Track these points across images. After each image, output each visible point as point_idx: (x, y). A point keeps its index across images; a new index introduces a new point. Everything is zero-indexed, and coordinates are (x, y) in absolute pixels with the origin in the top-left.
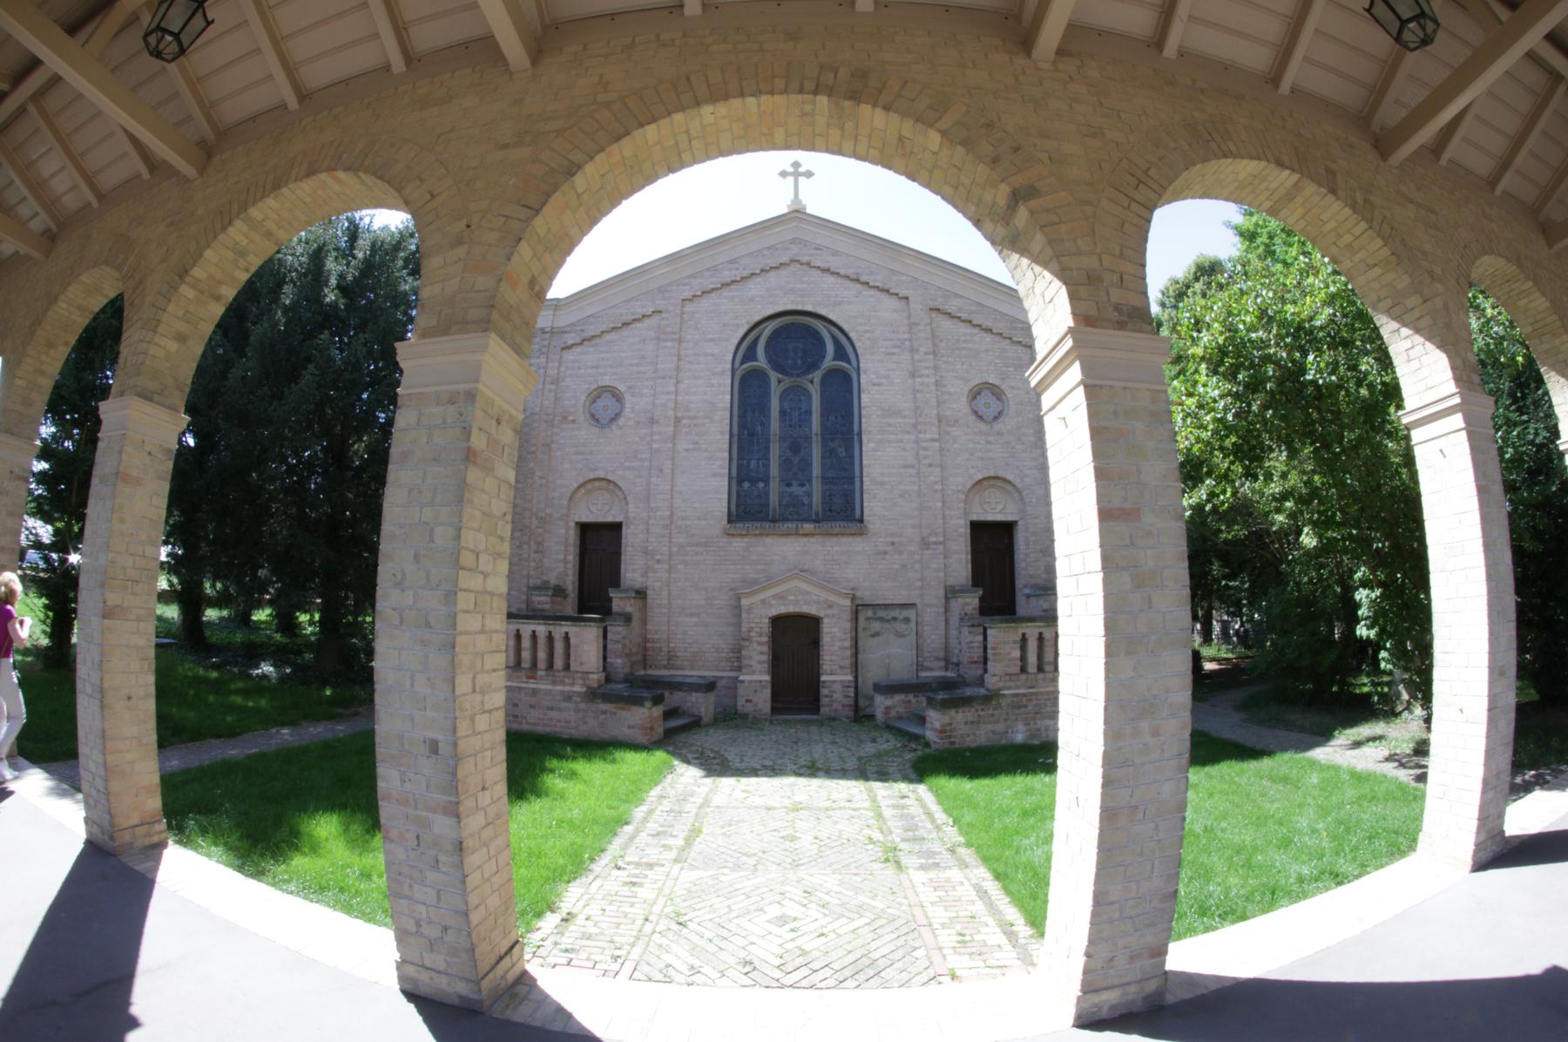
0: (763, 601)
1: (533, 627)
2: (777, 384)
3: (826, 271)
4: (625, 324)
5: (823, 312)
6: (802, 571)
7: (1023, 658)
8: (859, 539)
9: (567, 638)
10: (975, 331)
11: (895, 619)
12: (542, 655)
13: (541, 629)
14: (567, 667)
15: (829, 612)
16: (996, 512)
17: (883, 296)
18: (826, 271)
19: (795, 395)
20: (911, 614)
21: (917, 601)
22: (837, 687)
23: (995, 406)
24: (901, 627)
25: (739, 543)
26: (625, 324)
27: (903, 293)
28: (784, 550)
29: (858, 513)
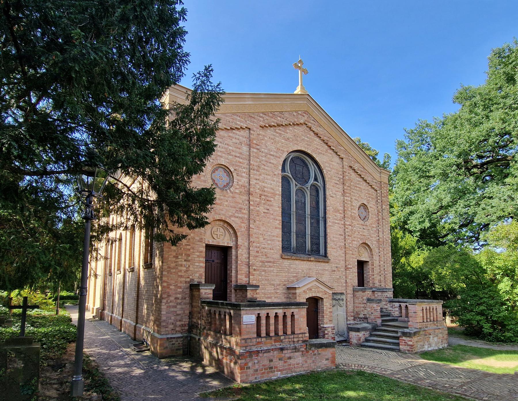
0: (304, 291)
1: (276, 311)
2: (294, 187)
3: (317, 134)
4: (232, 129)
5: (314, 156)
6: (309, 277)
7: (423, 316)
8: (327, 264)
9: (293, 315)
10: (361, 180)
11: (339, 299)
12: (281, 327)
13: (280, 312)
14: (293, 333)
15: (325, 296)
16: (364, 258)
17: (334, 154)
18: (317, 134)
19: (301, 192)
20: (344, 297)
21: (344, 292)
22: (330, 329)
23: (365, 214)
24: (341, 302)
25: (286, 263)
26: (232, 129)
27: (342, 156)
28: (301, 266)
29: (322, 251)
